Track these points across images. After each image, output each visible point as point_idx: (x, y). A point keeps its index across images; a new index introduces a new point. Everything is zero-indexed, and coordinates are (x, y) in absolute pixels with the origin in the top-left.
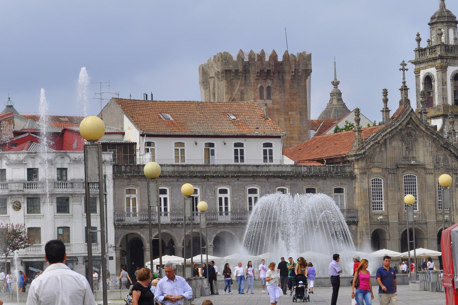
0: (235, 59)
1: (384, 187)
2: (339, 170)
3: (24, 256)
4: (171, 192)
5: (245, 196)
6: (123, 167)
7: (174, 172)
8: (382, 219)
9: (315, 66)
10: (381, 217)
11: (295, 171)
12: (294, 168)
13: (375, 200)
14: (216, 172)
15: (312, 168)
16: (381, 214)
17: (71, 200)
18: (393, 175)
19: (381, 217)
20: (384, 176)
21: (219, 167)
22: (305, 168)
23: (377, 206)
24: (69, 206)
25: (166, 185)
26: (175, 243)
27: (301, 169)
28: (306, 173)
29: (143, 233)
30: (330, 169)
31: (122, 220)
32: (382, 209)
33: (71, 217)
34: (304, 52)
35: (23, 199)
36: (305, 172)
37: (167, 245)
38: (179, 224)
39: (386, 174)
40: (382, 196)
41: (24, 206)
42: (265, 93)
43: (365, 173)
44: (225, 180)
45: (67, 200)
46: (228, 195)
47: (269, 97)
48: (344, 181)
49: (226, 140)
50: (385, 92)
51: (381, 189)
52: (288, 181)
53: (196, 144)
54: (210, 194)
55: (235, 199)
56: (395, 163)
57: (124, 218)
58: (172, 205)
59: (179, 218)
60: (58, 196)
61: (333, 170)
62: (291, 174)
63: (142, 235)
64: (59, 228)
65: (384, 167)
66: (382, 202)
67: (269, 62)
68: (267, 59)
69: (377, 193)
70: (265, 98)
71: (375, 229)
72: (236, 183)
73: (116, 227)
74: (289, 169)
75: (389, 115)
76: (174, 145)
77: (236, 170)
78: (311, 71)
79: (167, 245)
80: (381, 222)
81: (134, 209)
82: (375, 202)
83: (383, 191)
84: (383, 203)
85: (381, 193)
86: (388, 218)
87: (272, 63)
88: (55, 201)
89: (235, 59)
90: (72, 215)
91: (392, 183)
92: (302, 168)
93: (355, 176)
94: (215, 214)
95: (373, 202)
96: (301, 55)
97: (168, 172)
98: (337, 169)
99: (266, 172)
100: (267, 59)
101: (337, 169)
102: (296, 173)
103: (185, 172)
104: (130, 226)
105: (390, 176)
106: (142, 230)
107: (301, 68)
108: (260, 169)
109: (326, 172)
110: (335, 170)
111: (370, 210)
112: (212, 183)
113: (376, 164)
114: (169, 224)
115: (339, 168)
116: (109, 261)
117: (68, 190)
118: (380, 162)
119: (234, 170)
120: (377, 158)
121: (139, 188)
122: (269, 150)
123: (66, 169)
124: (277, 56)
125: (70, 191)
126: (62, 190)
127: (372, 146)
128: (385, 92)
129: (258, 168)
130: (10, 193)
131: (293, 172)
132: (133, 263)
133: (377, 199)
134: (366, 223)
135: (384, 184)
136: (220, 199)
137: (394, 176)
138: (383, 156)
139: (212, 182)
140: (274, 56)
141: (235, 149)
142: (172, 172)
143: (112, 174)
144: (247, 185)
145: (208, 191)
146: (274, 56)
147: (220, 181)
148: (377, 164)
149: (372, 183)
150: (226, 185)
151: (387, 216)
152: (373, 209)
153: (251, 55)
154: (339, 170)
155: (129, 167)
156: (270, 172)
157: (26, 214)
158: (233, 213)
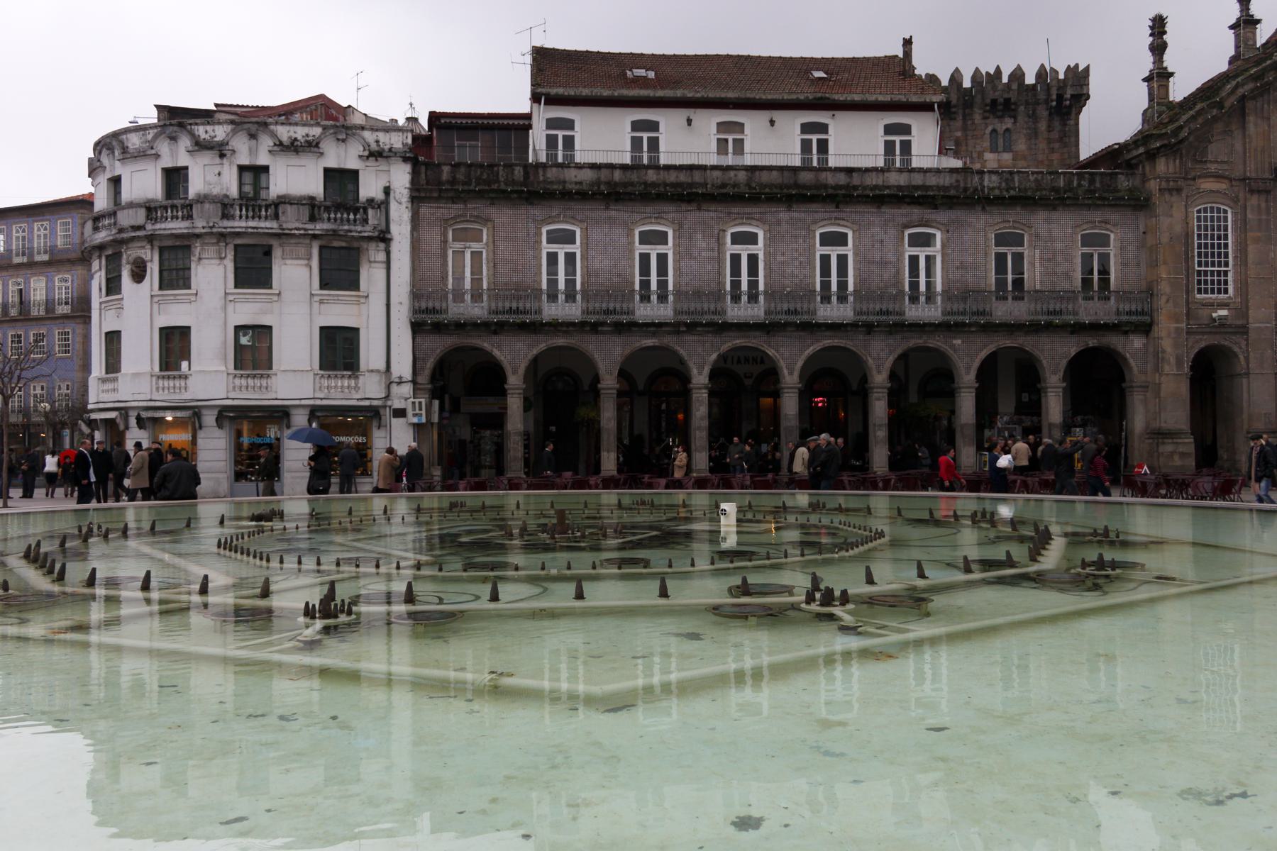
0: (945, 82)
1: (1234, 230)
2: (1098, 185)
3: (145, 404)
4: (586, 237)
5: (810, 250)
6: (446, 169)
7: (598, 182)
8: (1225, 317)
9: (1095, 85)
10: (1223, 312)
11: (962, 185)
12: (960, 177)
13: (1207, 265)
14: (724, 185)
15: (1016, 178)
16: (1223, 305)
17: (277, 253)
18: (1263, 197)
19: (1223, 312)
20: (1235, 200)
21: (732, 173)
22: (994, 178)
23: (1206, 282)
24: (271, 268)
25: (573, 220)
26: (1044, 410)
27: (982, 180)
28: (997, 192)
29: (499, 348)
30: (1071, 182)
31: (983, 313)
32: (1226, 291)
33: (275, 298)
34: (1077, 66)
35: (149, 252)
36: (993, 188)
37: (641, 387)
38: (603, 324)
39: (1241, 195)
40: (1226, 255)
41: (153, 269)
42: (1001, 142)
43: (1179, 190)
44: (753, 210)
45: (268, 252)
46: (759, 249)
47: (1007, 149)
48: (1109, 215)
49: (778, 115)
50: (1158, 26)
51: (1226, 237)
52: (942, 215)
53: (689, 122)
54: (704, 245)
55: (780, 258)
56: (1270, 163)
57: (444, 305)
58: (587, 274)
59: (611, 306)
60: (239, 241)
61: (1080, 185)
62: (953, 192)
63: (496, 353)
64: (239, 329)
65: (1237, 173)
66: (1226, 273)
67: (1008, 85)
68: (1005, 80)
69: (1212, 221)
70: (1000, 149)
71: (1203, 344)
72: (784, 215)
73: (417, 328)
74: (947, 180)
75: (1254, 34)
76: (715, 130)
77: (786, 181)
78: (1088, 98)
79: (641, 387)
80: (1220, 326)
81: (570, 283)
82: (1206, 272)
83: (1230, 241)
84: (1230, 274)
85: (1226, 246)
86: (1246, 316)
87: (1015, 86)
88: (230, 256)
89: (945, 82)
90: (279, 294)
91: (1260, 220)
92: (986, 177)
93: (1147, 199)
94: (718, 295)
95: (1199, 272)
96: (1072, 71)
97: (581, 183)
98: (1092, 182)
99: (876, 187)
100: (1005, 80)
101: (1092, 182)
102: (966, 189)
103: (632, 184)
104: (460, 326)
105: (1254, 200)
106: (496, 339)
107: (1069, 92)
108: (856, 180)
109: (1056, 190)
110: (1085, 183)
111: (1187, 293)
112: (712, 214)
113: (1213, 168)
114: (573, 324)
115: (1098, 179)
116: (394, 421)
117: (262, 224)
118: (1222, 162)
119: (780, 181)
120: (1216, 150)
121: (490, 225)
122: (901, 142)
123: (265, 169)
124: (1023, 74)
125: (271, 225)
126: (244, 224)
127: (1199, 113)
128: (1158, 26)
129: (851, 177)
130: (120, 236)
131: (957, 188)
132: (553, 429)
133: (1212, 212)
134: (1177, 329)
135: (1234, 222)
136: (736, 259)
137: (1267, 201)
138: (1233, 145)
139: (709, 214)
140: (1018, 75)
141: (886, 142)
142: (592, 184)
143: (408, 185)
144: (815, 222)
145: (699, 236)
146: (1018, 75)
147: (735, 210)
148: (1216, 166)
149: (1199, 218)
150: (754, 222)
151: (1242, 311)
152: (1199, 291)
153: (977, 74)
154: (1098, 185)
155: (463, 169)
156: (888, 187)
157: (156, 291)
158: (771, 294)
